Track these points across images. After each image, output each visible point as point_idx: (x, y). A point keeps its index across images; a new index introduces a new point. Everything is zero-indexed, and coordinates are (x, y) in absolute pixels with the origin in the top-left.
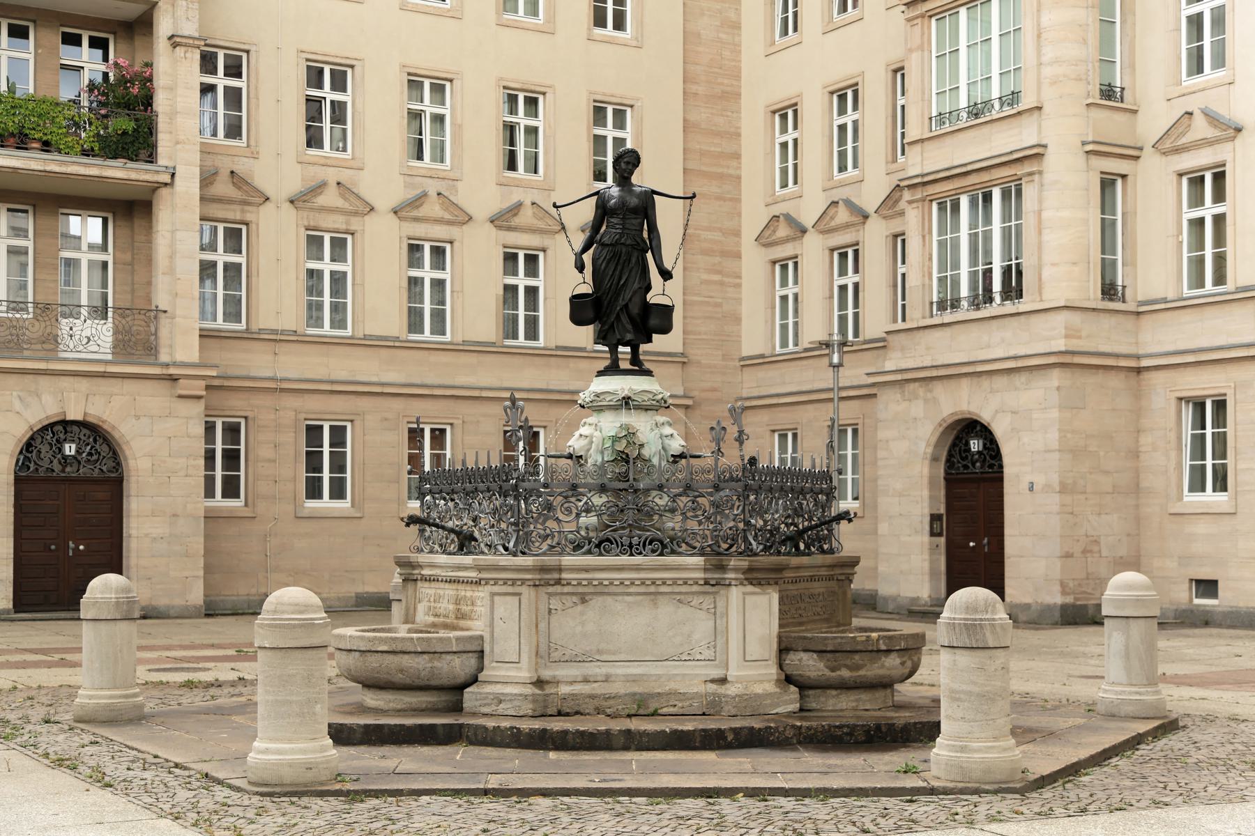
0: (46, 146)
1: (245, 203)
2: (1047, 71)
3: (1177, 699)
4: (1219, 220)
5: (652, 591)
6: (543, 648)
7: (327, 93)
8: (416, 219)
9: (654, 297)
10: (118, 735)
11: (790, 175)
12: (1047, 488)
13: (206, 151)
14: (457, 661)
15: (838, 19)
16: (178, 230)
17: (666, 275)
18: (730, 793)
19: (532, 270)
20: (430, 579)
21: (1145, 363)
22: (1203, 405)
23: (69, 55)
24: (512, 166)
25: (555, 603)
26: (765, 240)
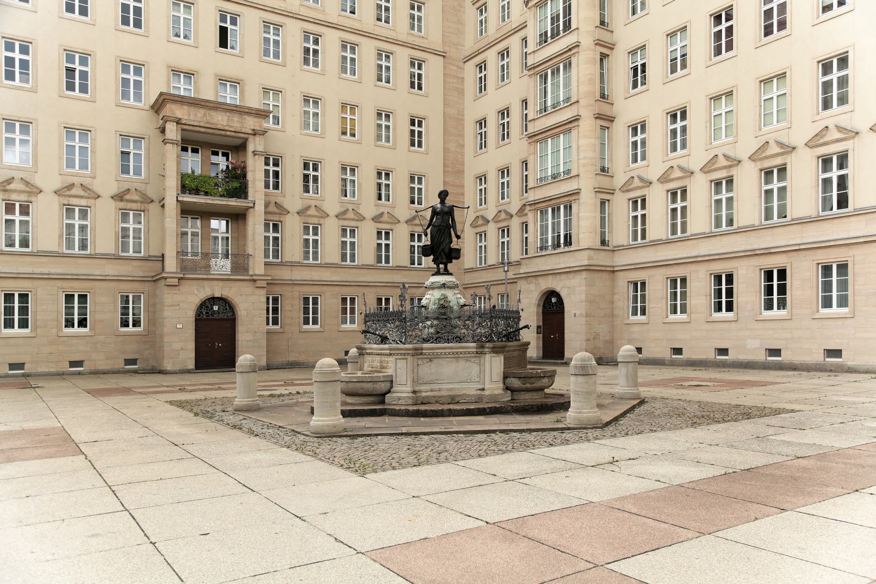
0: (206, 194)
1: (281, 214)
2: (581, 162)
3: (645, 392)
4: (644, 216)
5: (457, 356)
6: (415, 379)
7: (311, 173)
8: (345, 219)
9: (454, 245)
10: (254, 416)
11: (483, 201)
12: (581, 315)
13: (266, 195)
14: (383, 385)
15: (501, 143)
16: (256, 224)
17: (458, 237)
18: (494, 431)
19: (387, 238)
20: (368, 354)
21: (616, 269)
22: (637, 284)
23: (214, 159)
24: (380, 198)
25: (420, 362)
26: (473, 225)
